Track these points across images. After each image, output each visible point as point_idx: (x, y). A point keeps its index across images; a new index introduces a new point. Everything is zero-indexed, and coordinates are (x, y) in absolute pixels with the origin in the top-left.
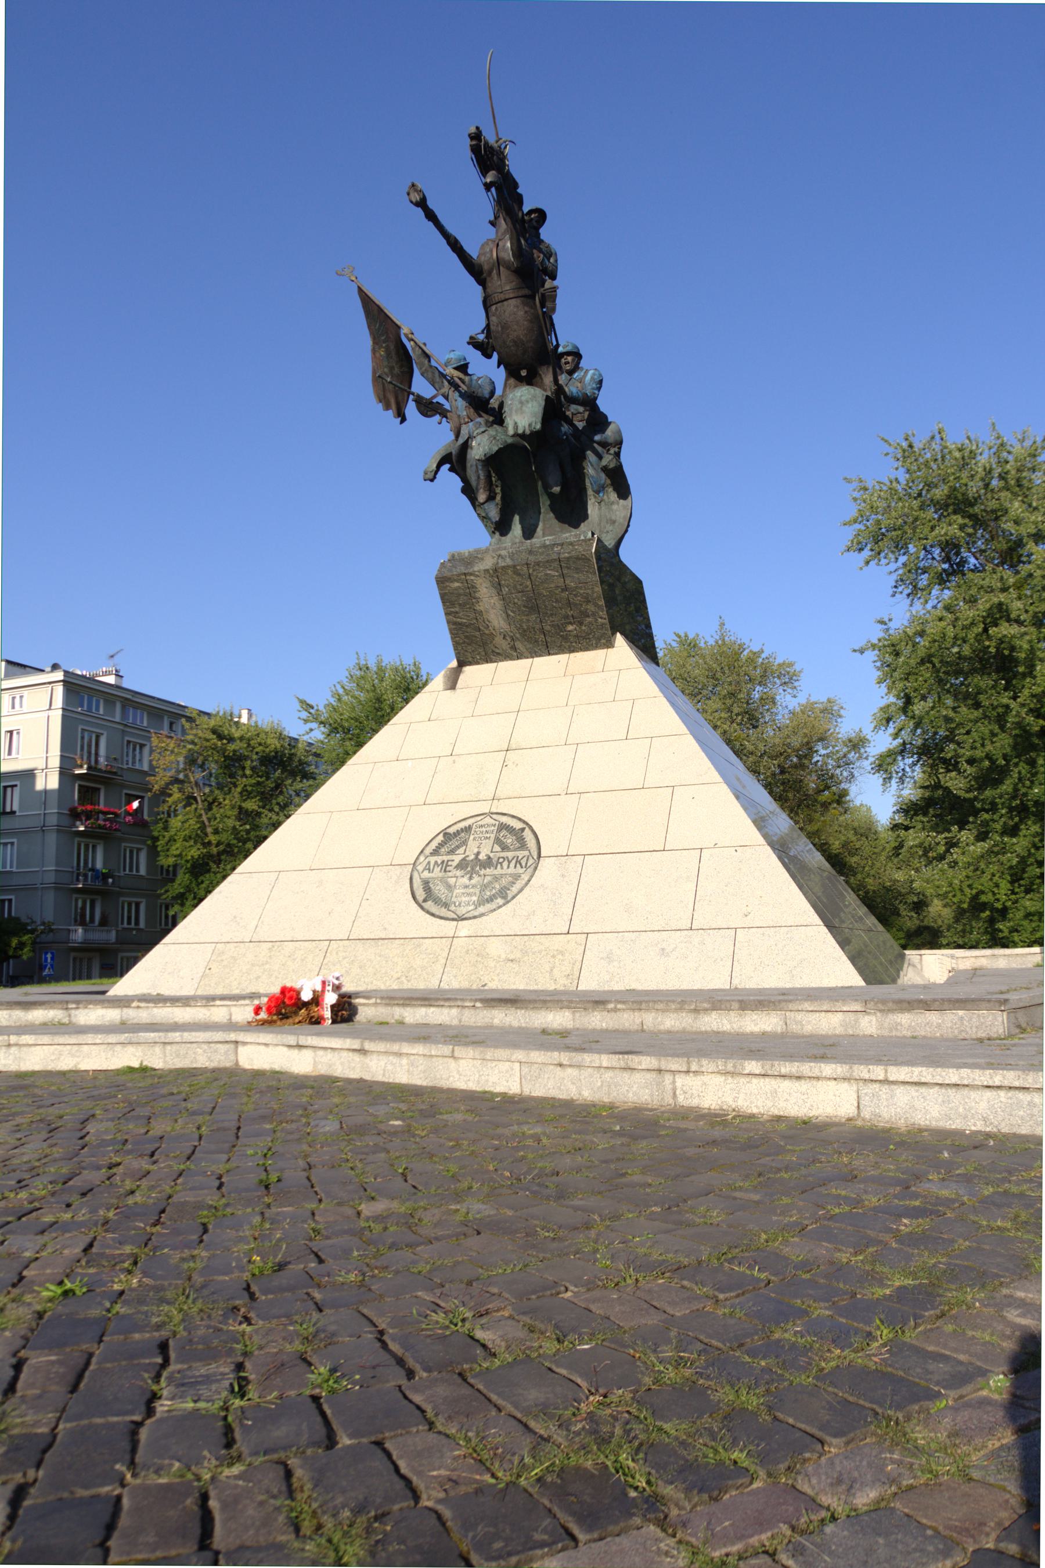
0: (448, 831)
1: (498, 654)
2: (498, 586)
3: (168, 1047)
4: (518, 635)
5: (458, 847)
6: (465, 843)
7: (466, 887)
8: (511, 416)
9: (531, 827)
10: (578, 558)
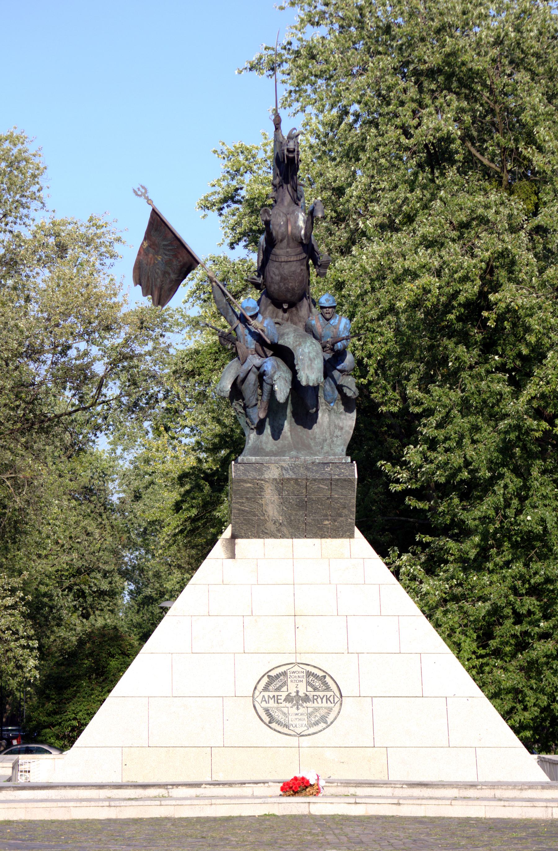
1: (266, 533)
2: (280, 492)
3: (280, 805)
4: (285, 523)
5: (281, 686)
6: (285, 683)
7: (297, 714)
8: (304, 369)
10: (345, 480)
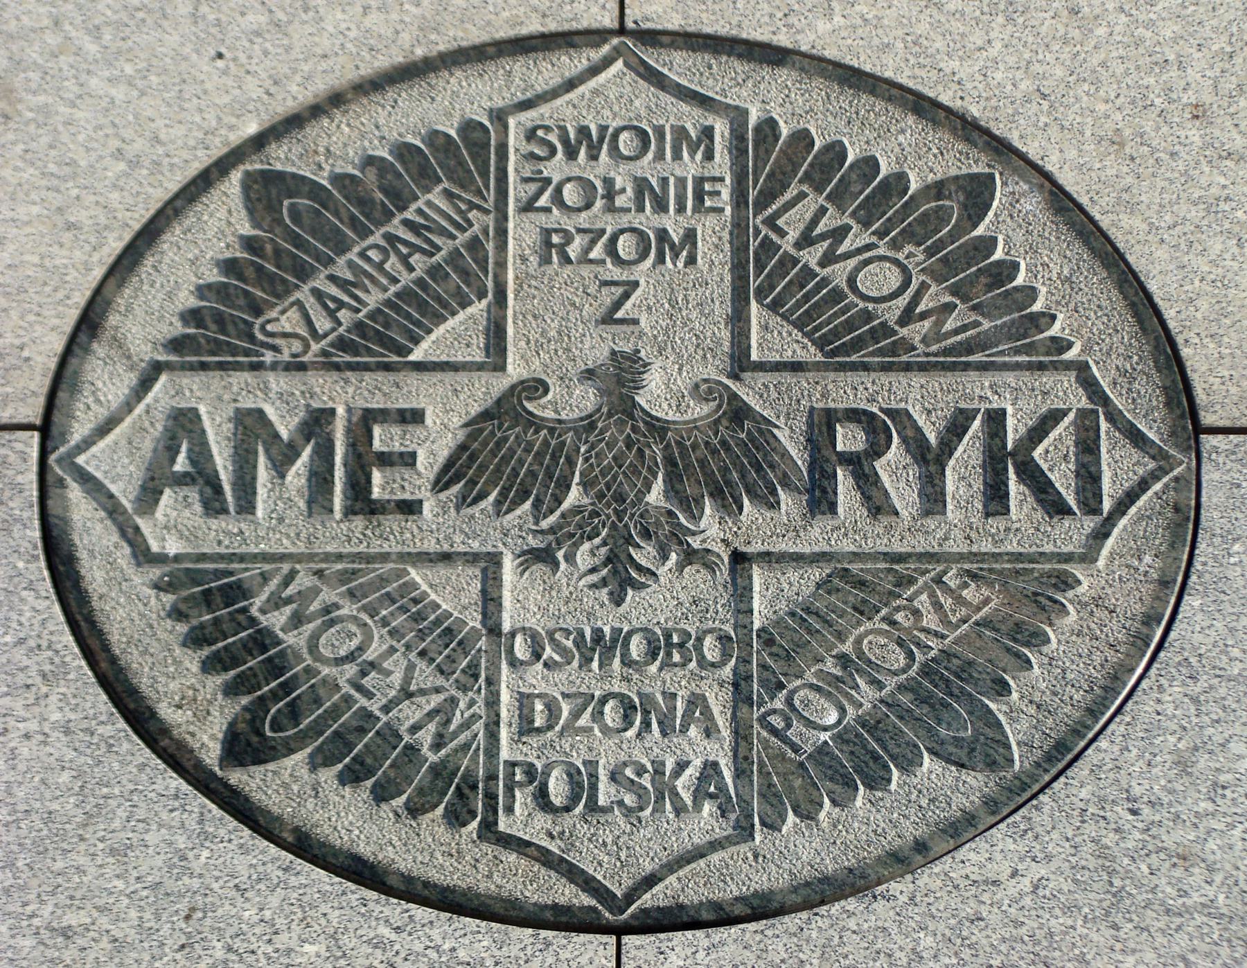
0: (283, 157)
5: (423, 306)
6: (471, 273)
9: (177, 758)
